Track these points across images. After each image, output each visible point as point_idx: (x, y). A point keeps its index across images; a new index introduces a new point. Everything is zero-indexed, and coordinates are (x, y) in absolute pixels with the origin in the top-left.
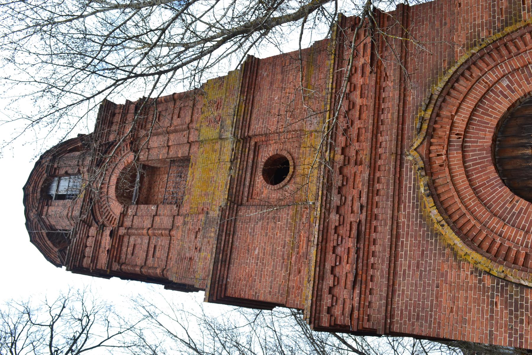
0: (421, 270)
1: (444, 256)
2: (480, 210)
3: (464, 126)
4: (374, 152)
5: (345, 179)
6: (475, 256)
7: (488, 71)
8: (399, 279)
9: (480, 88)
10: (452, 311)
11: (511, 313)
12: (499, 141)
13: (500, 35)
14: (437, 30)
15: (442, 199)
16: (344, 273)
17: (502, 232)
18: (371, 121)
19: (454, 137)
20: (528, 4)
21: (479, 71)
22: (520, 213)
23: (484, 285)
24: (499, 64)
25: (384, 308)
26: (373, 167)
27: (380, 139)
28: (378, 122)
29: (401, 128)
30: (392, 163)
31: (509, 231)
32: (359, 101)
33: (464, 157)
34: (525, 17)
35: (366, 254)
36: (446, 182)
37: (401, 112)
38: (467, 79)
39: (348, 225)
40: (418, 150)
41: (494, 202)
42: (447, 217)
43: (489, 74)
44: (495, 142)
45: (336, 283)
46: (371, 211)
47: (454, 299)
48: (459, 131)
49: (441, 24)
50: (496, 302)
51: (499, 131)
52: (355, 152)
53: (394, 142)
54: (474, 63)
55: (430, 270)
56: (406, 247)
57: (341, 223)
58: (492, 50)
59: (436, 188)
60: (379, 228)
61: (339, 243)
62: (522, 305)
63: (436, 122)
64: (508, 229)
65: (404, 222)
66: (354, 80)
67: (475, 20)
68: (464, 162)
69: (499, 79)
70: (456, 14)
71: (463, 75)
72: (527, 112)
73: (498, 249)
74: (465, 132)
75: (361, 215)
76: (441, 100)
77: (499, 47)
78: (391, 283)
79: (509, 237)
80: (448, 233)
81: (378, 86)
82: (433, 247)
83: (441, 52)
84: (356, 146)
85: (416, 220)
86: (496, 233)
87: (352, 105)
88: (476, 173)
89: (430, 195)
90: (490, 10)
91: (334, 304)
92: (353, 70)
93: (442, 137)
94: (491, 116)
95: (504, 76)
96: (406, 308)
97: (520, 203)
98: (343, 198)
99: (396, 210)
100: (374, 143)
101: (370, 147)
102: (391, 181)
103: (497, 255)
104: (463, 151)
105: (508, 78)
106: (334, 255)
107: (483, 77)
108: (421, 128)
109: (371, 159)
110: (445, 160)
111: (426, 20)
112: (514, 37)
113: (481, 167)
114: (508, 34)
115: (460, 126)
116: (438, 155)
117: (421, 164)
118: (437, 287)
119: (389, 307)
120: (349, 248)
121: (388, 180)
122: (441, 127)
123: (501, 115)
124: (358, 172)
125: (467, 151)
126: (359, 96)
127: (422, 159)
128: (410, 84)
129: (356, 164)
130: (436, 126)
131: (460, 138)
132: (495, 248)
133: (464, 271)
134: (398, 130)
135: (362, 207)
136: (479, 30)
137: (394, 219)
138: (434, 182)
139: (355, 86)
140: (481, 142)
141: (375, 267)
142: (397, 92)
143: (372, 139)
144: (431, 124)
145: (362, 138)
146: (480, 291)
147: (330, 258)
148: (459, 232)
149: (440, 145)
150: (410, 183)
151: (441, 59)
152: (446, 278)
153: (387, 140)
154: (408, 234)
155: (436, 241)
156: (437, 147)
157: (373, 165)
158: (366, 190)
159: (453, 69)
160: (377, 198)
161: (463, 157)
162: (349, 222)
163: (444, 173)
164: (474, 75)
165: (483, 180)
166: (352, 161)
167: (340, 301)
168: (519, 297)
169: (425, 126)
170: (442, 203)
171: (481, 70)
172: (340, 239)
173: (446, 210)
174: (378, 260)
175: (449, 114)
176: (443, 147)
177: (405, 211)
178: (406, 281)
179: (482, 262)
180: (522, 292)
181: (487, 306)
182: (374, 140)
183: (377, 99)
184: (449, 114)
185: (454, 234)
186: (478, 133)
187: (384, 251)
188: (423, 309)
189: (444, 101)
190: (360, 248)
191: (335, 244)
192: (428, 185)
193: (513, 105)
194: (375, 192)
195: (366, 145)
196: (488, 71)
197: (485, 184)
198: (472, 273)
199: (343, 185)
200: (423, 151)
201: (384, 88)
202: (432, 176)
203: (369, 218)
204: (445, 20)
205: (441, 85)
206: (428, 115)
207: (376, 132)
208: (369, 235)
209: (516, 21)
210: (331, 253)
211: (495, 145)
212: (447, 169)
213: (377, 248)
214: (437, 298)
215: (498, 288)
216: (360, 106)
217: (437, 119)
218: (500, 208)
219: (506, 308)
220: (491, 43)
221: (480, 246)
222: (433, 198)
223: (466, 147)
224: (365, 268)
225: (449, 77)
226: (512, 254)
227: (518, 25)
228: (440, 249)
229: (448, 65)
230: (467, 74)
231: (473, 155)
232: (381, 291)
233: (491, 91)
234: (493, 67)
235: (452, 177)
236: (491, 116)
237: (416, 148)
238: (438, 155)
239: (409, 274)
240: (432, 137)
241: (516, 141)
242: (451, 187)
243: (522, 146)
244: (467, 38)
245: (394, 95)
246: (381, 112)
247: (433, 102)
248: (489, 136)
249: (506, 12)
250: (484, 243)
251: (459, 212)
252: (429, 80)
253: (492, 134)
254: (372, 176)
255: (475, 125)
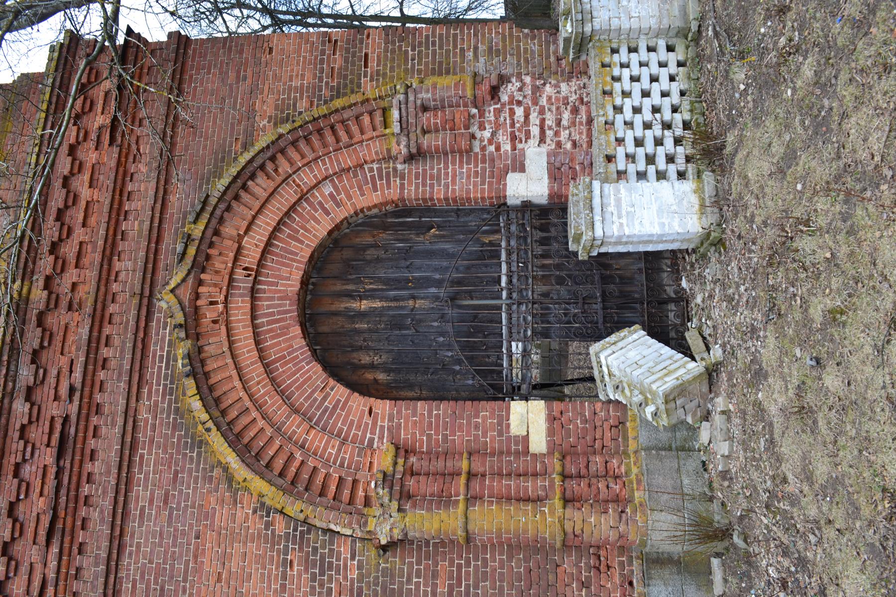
0: (171, 507)
1: (210, 482)
2: (273, 403)
3: (258, 256)
4: (103, 289)
5: (47, 334)
6: (258, 484)
7: (303, 166)
8: (133, 524)
9: (288, 193)
10: (219, 580)
11: (313, 579)
12: (313, 284)
13: (324, 110)
14: (231, 86)
15: (212, 381)
16: (34, 514)
17: (306, 440)
18: (102, 232)
19: (240, 274)
20: (372, 67)
21: (288, 165)
22: (335, 407)
23: (273, 531)
24: (320, 157)
25: (102, 580)
26: (99, 318)
27: (117, 265)
28: (115, 234)
29: (153, 250)
30: (133, 312)
31: (316, 440)
32: (85, 193)
33: (253, 308)
34: (366, 88)
35: (74, 479)
36: (220, 351)
37: (157, 221)
38: (269, 177)
39: (47, 424)
40: (177, 292)
41: (297, 389)
42: (216, 413)
43: (305, 172)
44: (307, 285)
45: (17, 535)
46: (91, 397)
47: (224, 558)
48: (249, 263)
49: (238, 77)
50: (291, 561)
51: (313, 268)
52: (69, 286)
53: (139, 275)
54: (282, 151)
55: (186, 506)
56: (148, 465)
57: (34, 419)
58: (311, 133)
59: (203, 362)
60: (103, 430)
61: (28, 456)
62: (331, 563)
63: (211, 245)
64: (315, 436)
65: (146, 420)
66: (80, 154)
67: (291, 80)
68: (253, 318)
69: (320, 182)
70: (263, 65)
71: (262, 167)
72: (358, 240)
73: (298, 470)
74: (258, 266)
75: (70, 406)
76: (222, 206)
77: (322, 129)
78: (117, 533)
79: (315, 450)
80: (217, 442)
81: (121, 170)
82: (193, 466)
83: (233, 124)
84: (71, 275)
85: (168, 417)
86: (296, 443)
87: (72, 198)
88: (272, 338)
89: (193, 374)
90: (315, 67)
91: (12, 574)
92: (81, 135)
93: (220, 272)
94: (302, 242)
95: (326, 178)
96: (142, 576)
97: (337, 391)
98: (41, 371)
99: (134, 398)
100: (104, 273)
101: (97, 279)
102: (129, 345)
103: (293, 482)
104: (253, 298)
105: (332, 181)
106: (16, 481)
107: (294, 176)
108: (184, 253)
109: (96, 301)
110: (222, 313)
111: (215, 66)
112: (345, 116)
113: (280, 328)
114: (337, 111)
115: (251, 256)
116: (212, 303)
117: (180, 318)
118: (197, 537)
119: (112, 577)
120: (45, 466)
121: (124, 343)
122: (220, 254)
123: (317, 241)
124: (73, 324)
125: (260, 299)
126: (87, 184)
127: (183, 309)
128: (179, 173)
129: (70, 308)
130: (213, 252)
131: (249, 275)
132: (293, 470)
133: (243, 507)
134: (147, 252)
135: (72, 390)
136: (295, 97)
137: (130, 415)
138: (200, 350)
139: (81, 164)
140: (283, 285)
141: (91, 503)
142: (153, 184)
143: (102, 266)
144: (203, 247)
145: (85, 261)
146: (266, 542)
147: (7, 486)
148: (235, 441)
149: (215, 285)
150: (162, 349)
151: (231, 137)
152: (213, 522)
153: (129, 267)
154: (152, 441)
155: (199, 454)
156: (211, 289)
157: (98, 312)
158: (82, 359)
159: (247, 156)
160: (102, 375)
161: (252, 308)
162: (49, 417)
163: (219, 335)
164: (280, 170)
165: (282, 350)
166: (64, 303)
167: (24, 569)
168: (327, 551)
169: (192, 251)
170: (211, 389)
171: (291, 163)
172: (29, 449)
173: (217, 401)
174: (97, 490)
175: (235, 233)
176: (221, 289)
177: (149, 399)
178: (144, 529)
179: (270, 495)
180: (331, 543)
181: (277, 569)
182: (105, 267)
183: (118, 193)
184: (235, 233)
185: (226, 445)
186: (279, 270)
187: (108, 472)
188: (171, 577)
189: (228, 209)
190: (64, 467)
191: (19, 460)
192: (189, 356)
193: (337, 227)
194: (101, 363)
195: (91, 275)
196: (303, 166)
197: (284, 357)
198: (255, 512)
199: (42, 347)
200: (186, 294)
201: (132, 174)
202: (198, 340)
203: (84, 412)
204: (245, 71)
205: (225, 181)
206: (197, 231)
207: (110, 252)
208: (84, 443)
209: (352, 92)
210: (10, 477)
211: (306, 292)
212: (223, 328)
213: (96, 468)
214: (196, 557)
215: (295, 536)
216: (88, 202)
217: (214, 239)
218: (306, 400)
219: (306, 570)
220: (310, 122)
221: (268, 466)
222: (195, 379)
223: (258, 291)
224: (71, 505)
225: (239, 169)
226: (319, 480)
227: (353, 99)
228: (204, 469)
229: (242, 148)
230: (269, 167)
231: (269, 307)
232: (99, 548)
233: (305, 200)
234: (310, 162)
235: (231, 344)
236: (302, 242)
237: (174, 288)
238: (212, 303)
239: (150, 514)
240: (203, 270)
241: (339, 287)
242: (229, 360)
243: (346, 296)
244: (276, 108)
245: (146, 190)
246: (122, 218)
247: (209, 209)
248: (297, 276)
249: (339, 74)
250: (276, 460)
251: (239, 405)
252: (209, 170)
253: (301, 273)
254: (95, 334)
255: (277, 255)
